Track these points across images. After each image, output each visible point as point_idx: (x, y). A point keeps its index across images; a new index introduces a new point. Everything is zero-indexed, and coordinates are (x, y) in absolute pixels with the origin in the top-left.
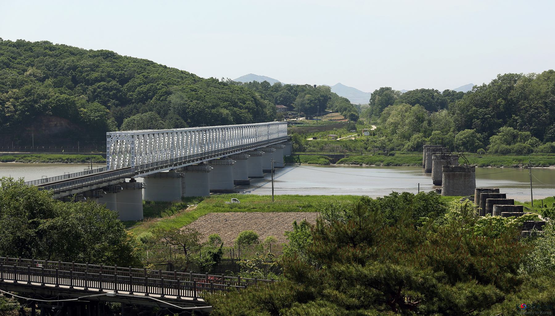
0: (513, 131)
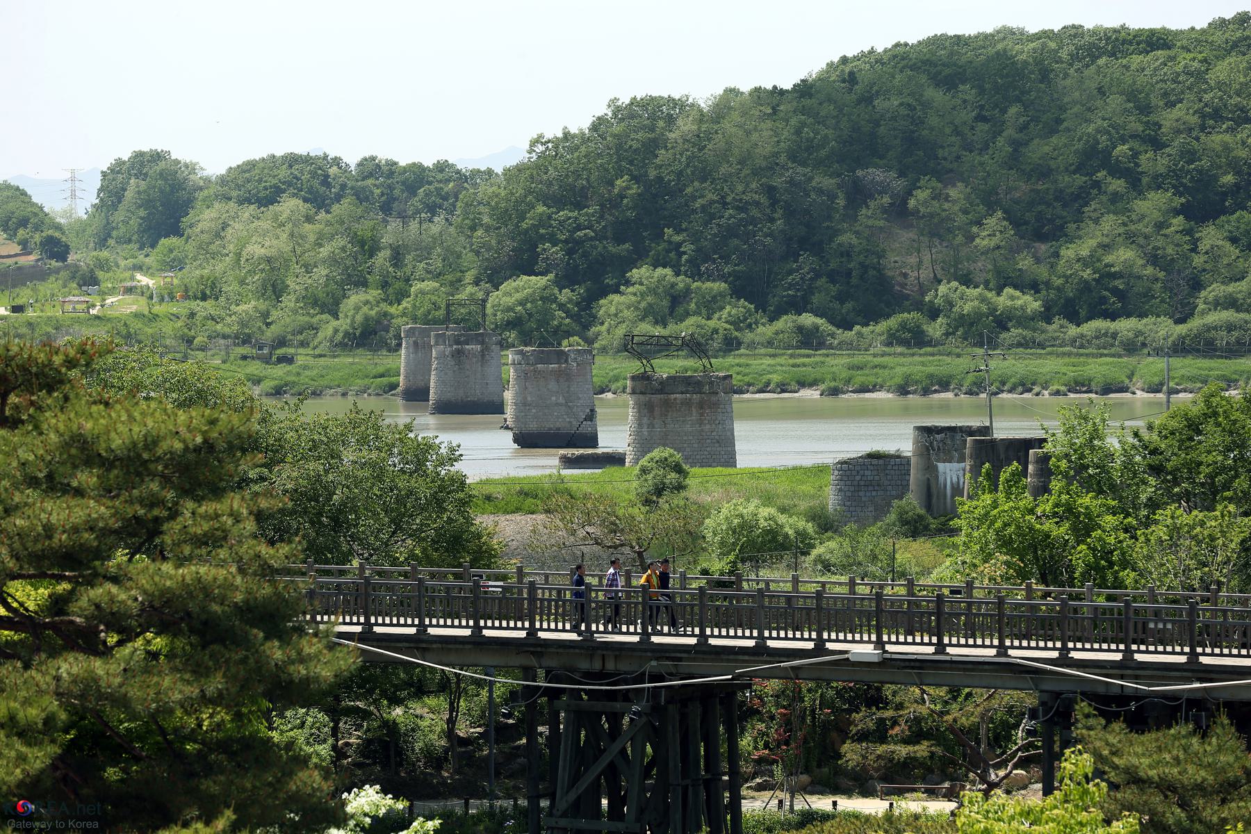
0: (673, 280)
